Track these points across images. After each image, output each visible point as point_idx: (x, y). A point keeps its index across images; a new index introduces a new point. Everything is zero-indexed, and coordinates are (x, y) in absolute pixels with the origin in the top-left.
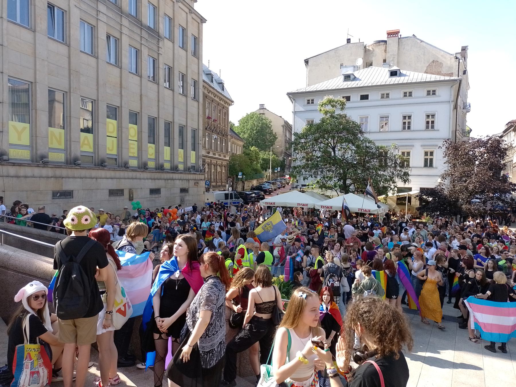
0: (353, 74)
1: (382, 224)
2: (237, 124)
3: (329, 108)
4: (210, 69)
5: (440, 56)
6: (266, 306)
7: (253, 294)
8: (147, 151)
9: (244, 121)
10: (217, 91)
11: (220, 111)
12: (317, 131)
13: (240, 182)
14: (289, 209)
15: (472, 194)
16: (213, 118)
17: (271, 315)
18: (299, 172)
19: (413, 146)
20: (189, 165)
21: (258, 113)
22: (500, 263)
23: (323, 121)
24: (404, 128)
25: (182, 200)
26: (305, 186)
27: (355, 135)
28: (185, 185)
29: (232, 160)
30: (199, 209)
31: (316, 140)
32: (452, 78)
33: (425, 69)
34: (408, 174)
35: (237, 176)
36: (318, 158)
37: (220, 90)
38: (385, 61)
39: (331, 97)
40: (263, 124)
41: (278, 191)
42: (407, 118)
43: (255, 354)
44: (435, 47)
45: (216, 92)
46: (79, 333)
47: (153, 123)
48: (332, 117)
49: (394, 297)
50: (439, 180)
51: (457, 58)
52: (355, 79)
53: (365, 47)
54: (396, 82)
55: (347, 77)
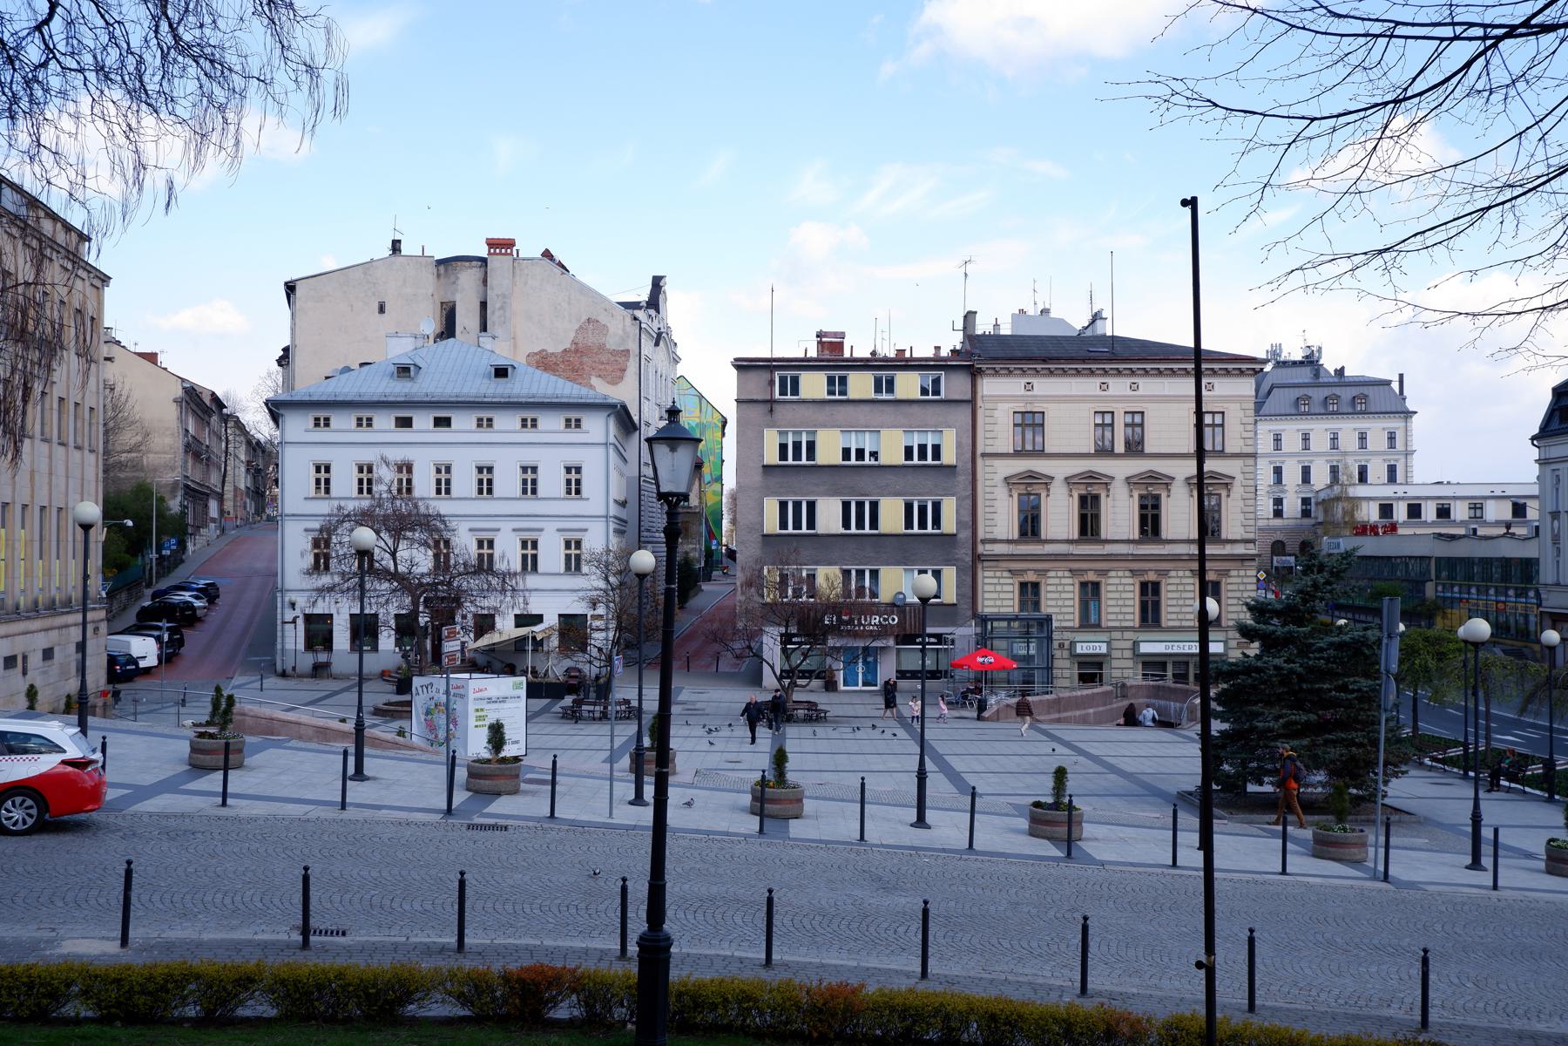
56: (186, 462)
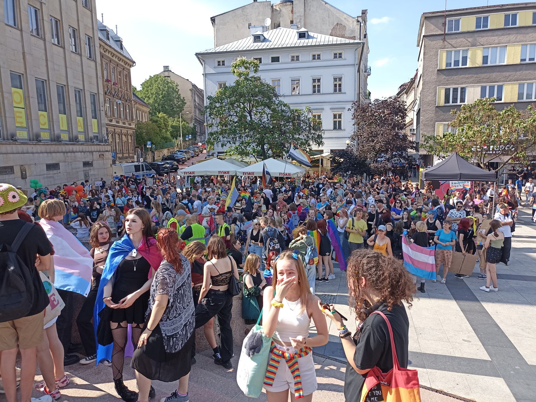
0: (262, 35)
1: (302, 187)
2: (139, 88)
3: (242, 70)
4: (104, 24)
5: (343, 19)
6: (223, 278)
7: (208, 267)
8: (38, 120)
9: (147, 85)
10: (115, 50)
11: (120, 72)
12: (233, 95)
13: (150, 153)
14: (206, 178)
15: (378, 153)
16: (113, 81)
17: (229, 287)
18: (217, 139)
19: (323, 109)
20: (91, 135)
21: (162, 75)
22: (412, 214)
23: (238, 83)
24: (314, 92)
25: (86, 175)
26: (223, 153)
27: (270, 98)
28: (88, 159)
29: (139, 128)
30: (108, 183)
31: (232, 104)
32: (356, 41)
33: (330, 31)
34: (321, 136)
35: (145, 145)
36: (235, 123)
37: (118, 49)
38: (292, 22)
39: (244, 58)
40: (169, 87)
41: (192, 160)
42: (317, 81)
43: (210, 328)
44: (339, 10)
45: (114, 52)
46: (21, 335)
47: (42, 87)
48: (246, 79)
49: (328, 254)
50: (348, 142)
51: (358, 22)
52: (265, 40)
53: (272, 7)
54: (305, 45)
55: (257, 38)
56: (195, 111)
